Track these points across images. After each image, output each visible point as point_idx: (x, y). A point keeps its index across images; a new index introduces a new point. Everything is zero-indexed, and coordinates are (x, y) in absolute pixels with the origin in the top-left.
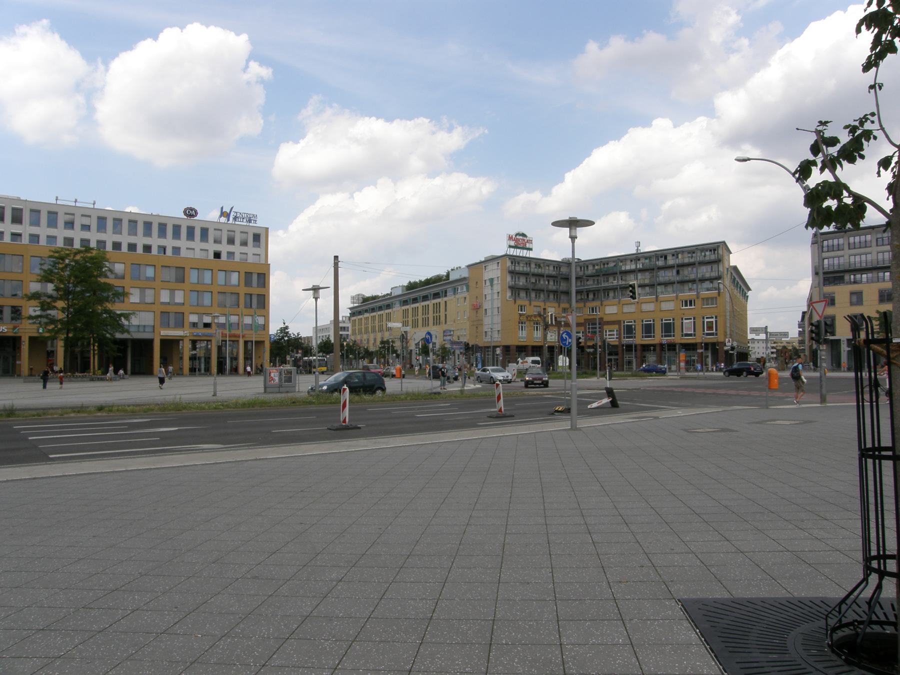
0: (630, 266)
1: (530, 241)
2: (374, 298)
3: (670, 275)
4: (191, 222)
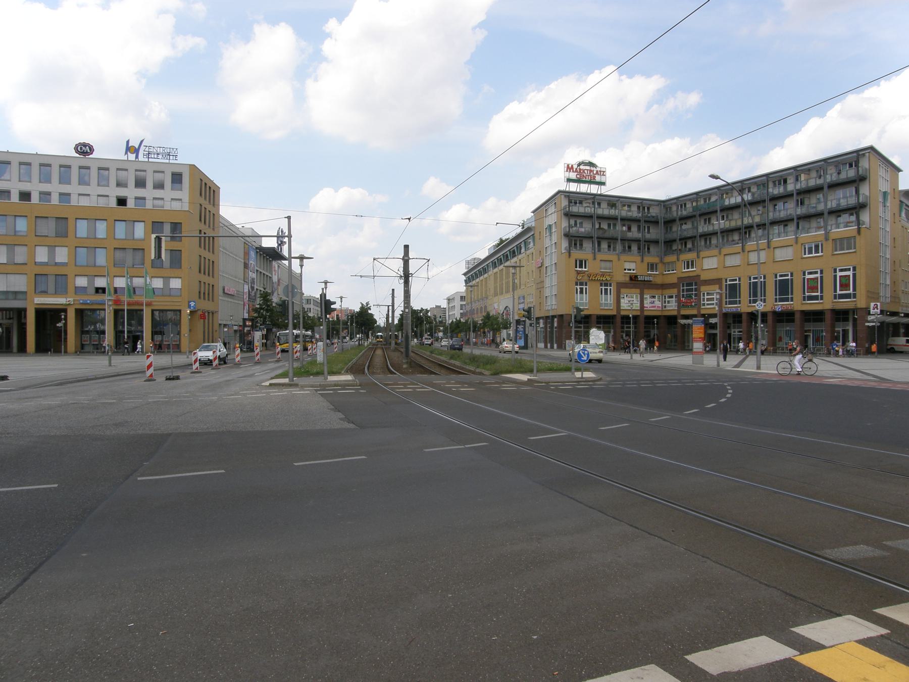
0: (735, 199)
1: (602, 173)
3: (788, 209)
4: (84, 161)
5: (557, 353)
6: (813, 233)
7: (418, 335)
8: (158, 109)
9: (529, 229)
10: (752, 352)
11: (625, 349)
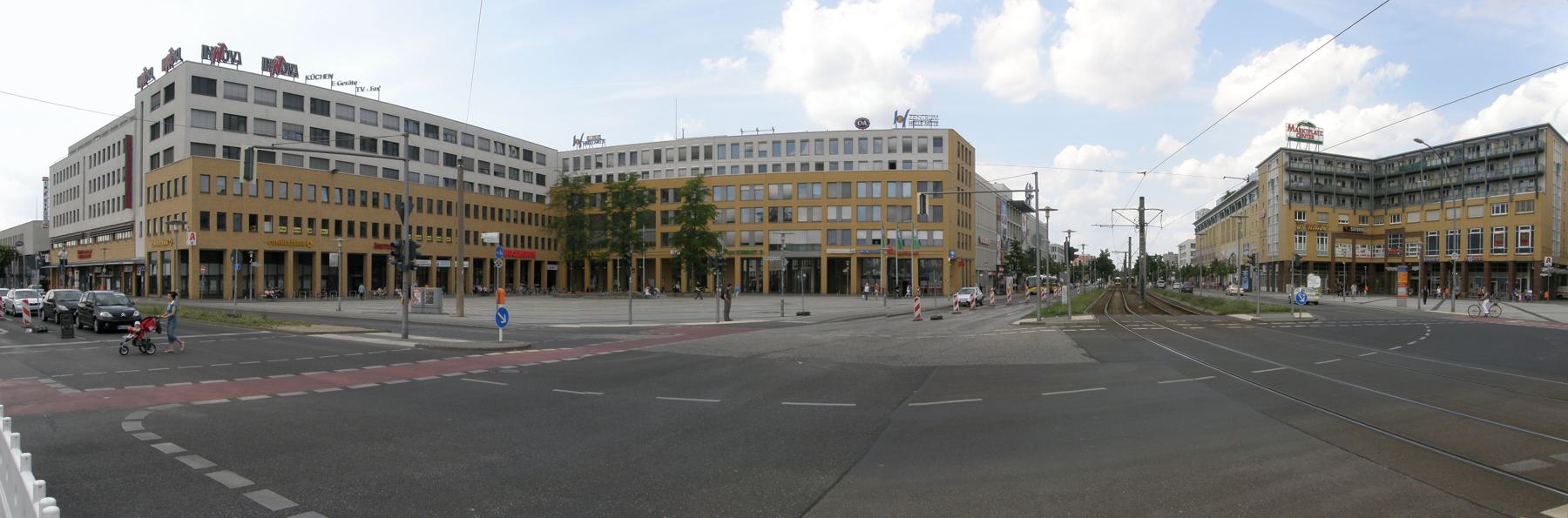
0: (1436, 162)
1: (1320, 133)
2: (613, 228)
3: (1480, 173)
4: (863, 134)
5: (1278, 296)
6: (1500, 196)
7: (1153, 279)
8: (921, 81)
9: (1253, 183)
10: (1448, 297)
11: (1339, 293)
